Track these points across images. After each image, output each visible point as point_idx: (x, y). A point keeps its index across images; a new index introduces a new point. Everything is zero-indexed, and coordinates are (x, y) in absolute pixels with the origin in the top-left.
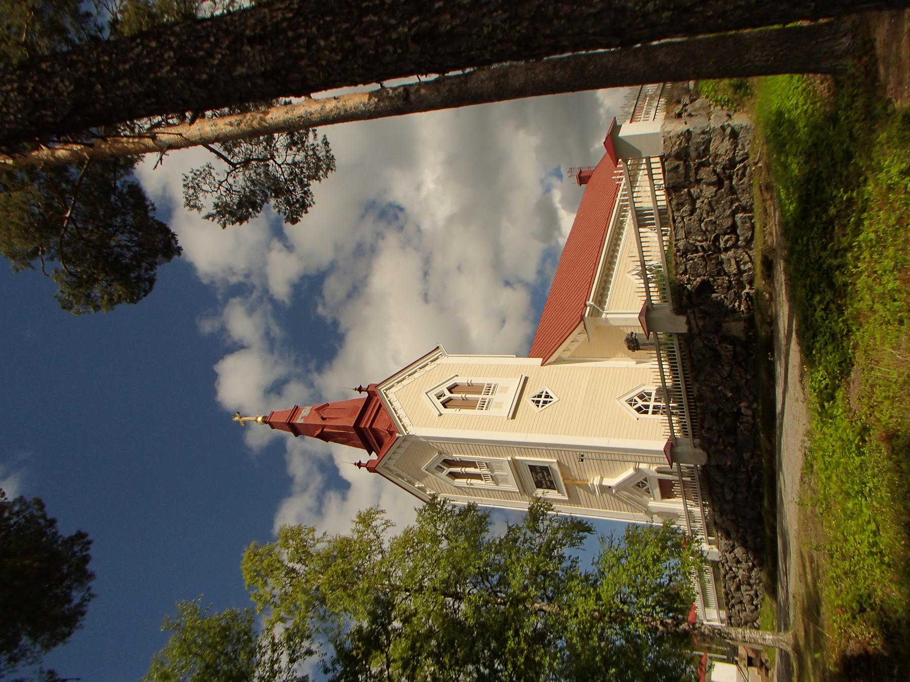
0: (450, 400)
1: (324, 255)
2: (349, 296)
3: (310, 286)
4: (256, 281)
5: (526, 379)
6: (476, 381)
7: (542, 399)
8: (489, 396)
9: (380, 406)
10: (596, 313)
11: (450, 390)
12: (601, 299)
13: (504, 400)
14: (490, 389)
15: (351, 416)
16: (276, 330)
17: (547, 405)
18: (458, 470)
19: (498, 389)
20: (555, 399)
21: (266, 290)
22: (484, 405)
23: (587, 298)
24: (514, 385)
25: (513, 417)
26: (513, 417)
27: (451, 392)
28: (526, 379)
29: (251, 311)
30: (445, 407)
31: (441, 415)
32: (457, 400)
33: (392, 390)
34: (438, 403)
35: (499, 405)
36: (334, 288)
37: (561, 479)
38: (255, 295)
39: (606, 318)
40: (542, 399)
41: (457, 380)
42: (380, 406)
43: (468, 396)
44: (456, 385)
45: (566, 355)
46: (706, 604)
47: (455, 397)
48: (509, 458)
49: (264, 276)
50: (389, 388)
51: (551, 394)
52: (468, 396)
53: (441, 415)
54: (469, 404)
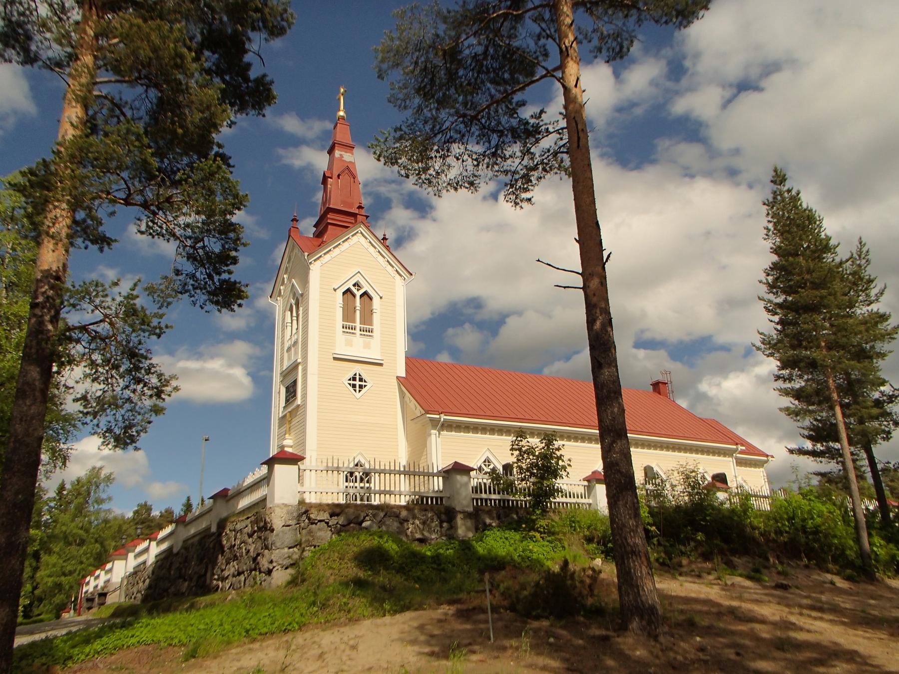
0: (354, 296)
1: (724, 140)
2: (686, 168)
3: (691, 130)
4: (684, 82)
5: (381, 365)
6: (376, 318)
7: (357, 383)
8: (358, 331)
9: (347, 227)
10: (434, 423)
11: (365, 294)
12: (449, 426)
13: (357, 346)
14: (368, 332)
15: (343, 202)
16: (639, 111)
17: (351, 388)
18: (294, 314)
19: (367, 339)
20: (358, 395)
21: (677, 93)
22: (348, 329)
23: (446, 413)
24: (373, 354)
25: (335, 359)
26: (335, 359)
27: (361, 296)
28: (381, 365)
29: (653, 83)
30: (344, 293)
31: (335, 290)
32: (355, 302)
33: (362, 239)
34: (350, 285)
35: (349, 344)
36: (690, 153)
37: (290, 410)
38: (669, 84)
39: (430, 435)
40: (357, 383)
41: (376, 299)
42: (347, 227)
43: (358, 313)
44: (371, 298)
45: (407, 399)
46: (136, 556)
47: (357, 303)
48: (299, 360)
49: (692, 89)
50: (363, 235)
51: (364, 390)
52: (358, 313)
53: (335, 290)
54: (348, 315)
